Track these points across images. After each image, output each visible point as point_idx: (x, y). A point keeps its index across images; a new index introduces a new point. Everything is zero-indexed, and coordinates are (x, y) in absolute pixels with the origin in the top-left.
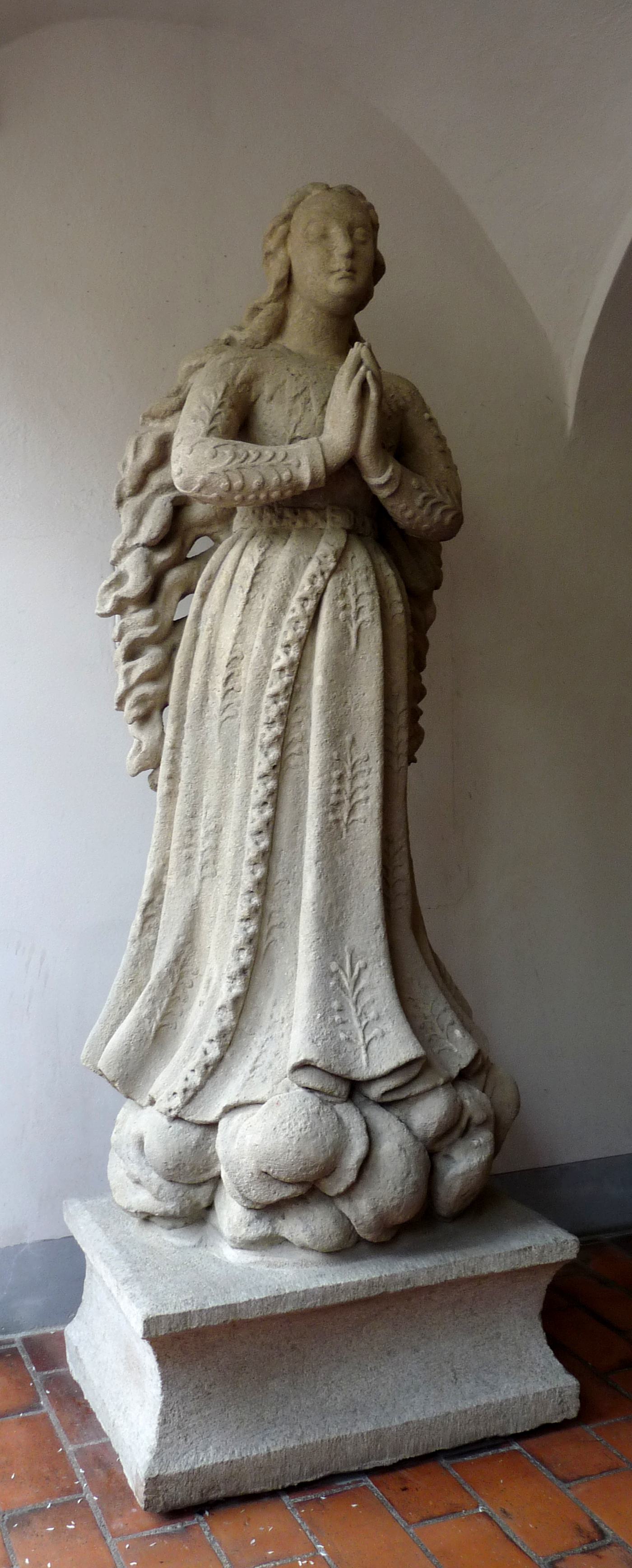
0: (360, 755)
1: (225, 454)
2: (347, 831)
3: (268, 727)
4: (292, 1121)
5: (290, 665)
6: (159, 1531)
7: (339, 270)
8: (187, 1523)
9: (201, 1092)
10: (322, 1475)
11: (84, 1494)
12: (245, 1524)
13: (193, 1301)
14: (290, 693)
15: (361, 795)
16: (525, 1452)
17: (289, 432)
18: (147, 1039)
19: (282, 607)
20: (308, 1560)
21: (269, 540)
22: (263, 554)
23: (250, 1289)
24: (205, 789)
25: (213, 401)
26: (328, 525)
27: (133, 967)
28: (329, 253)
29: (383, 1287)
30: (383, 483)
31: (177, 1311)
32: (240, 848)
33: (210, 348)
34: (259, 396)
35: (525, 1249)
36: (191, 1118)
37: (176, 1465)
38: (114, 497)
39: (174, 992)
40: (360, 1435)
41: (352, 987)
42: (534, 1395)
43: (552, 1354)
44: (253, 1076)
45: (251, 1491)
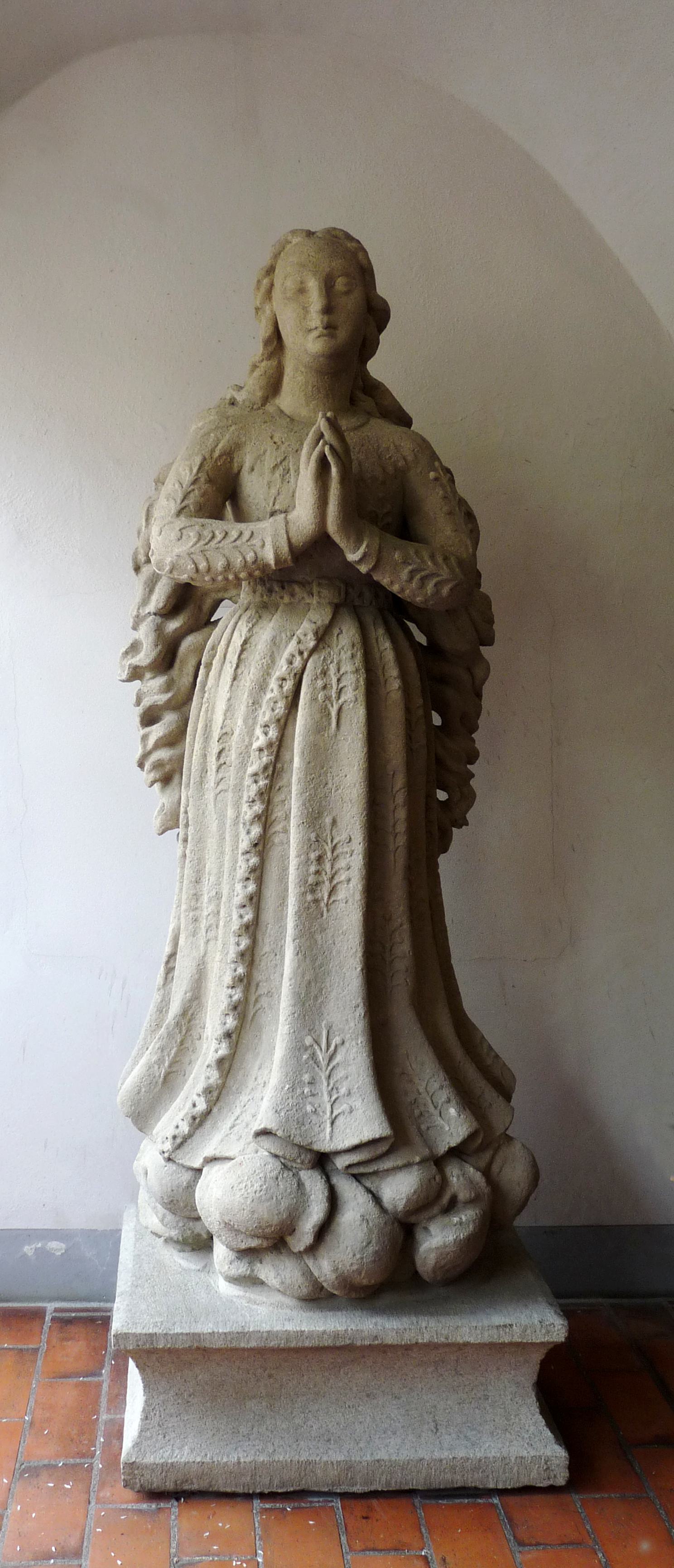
0: (343, 837)
1: (189, 537)
2: (328, 911)
3: (249, 806)
4: (249, 1183)
5: (267, 746)
6: (136, 1506)
7: (316, 328)
8: (162, 1505)
9: (190, 1140)
10: (292, 1489)
11: (94, 1460)
12: (209, 1518)
13: (162, 1324)
14: (270, 772)
15: (342, 876)
16: (501, 1508)
17: (269, 505)
18: (156, 1082)
19: (262, 686)
20: (242, 1562)
21: (257, 615)
22: (250, 630)
23: (218, 1322)
24: (207, 857)
25: (187, 479)
26: (314, 601)
27: (158, 1013)
28: (306, 310)
29: (349, 1339)
30: (357, 559)
31: (144, 1331)
32: (228, 919)
33: (213, 410)
34: (242, 467)
35: (505, 1326)
36: (180, 1161)
37: (152, 1457)
38: (130, 565)
39: (182, 1043)
40: (329, 1462)
41: (326, 1062)
42: (516, 1458)
43: (544, 1423)
44: (231, 1134)
45: (222, 1489)
